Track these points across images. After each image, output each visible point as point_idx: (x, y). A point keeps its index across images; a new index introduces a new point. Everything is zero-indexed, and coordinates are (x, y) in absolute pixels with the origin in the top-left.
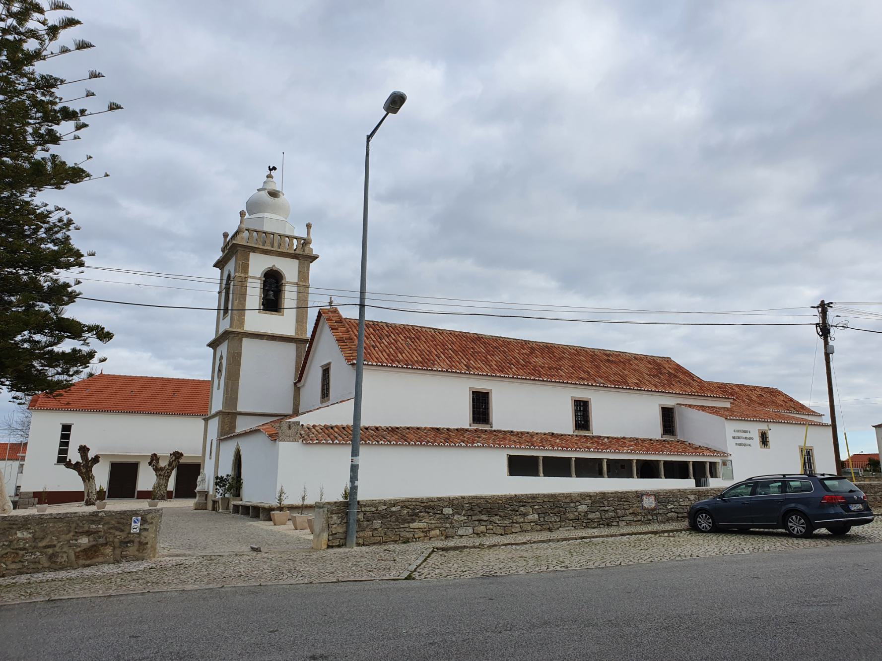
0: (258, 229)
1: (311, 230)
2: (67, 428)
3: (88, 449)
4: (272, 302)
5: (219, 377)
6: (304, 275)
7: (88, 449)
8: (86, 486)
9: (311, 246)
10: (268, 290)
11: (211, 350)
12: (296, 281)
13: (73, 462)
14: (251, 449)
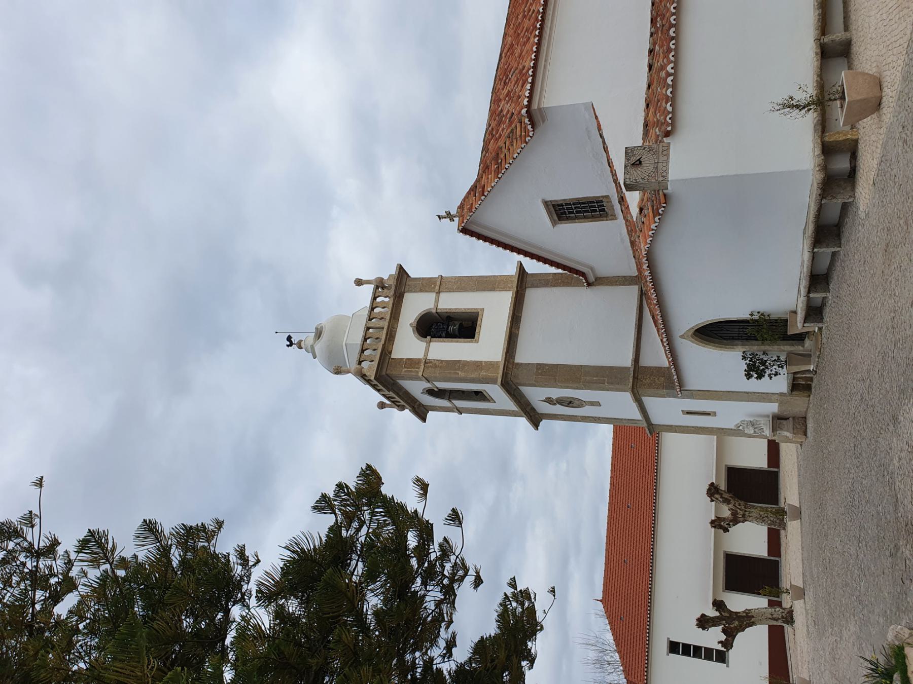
0: (358, 349)
1: (364, 278)
2: (674, 647)
3: (703, 615)
4: (464, 326)
5: (580, 404)
6: (426, 285)
7: (703, 615)
8: (761, 622)
9: (386, 278)
10: (447, 332)
11: (543, 423)
12: (434, 294)
13: (723, 637)
14: (692, 307)
